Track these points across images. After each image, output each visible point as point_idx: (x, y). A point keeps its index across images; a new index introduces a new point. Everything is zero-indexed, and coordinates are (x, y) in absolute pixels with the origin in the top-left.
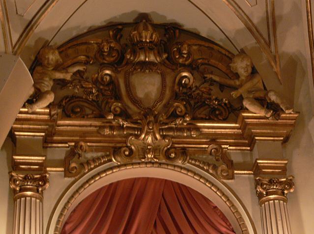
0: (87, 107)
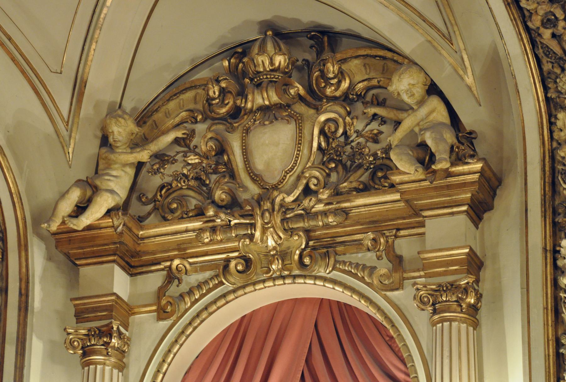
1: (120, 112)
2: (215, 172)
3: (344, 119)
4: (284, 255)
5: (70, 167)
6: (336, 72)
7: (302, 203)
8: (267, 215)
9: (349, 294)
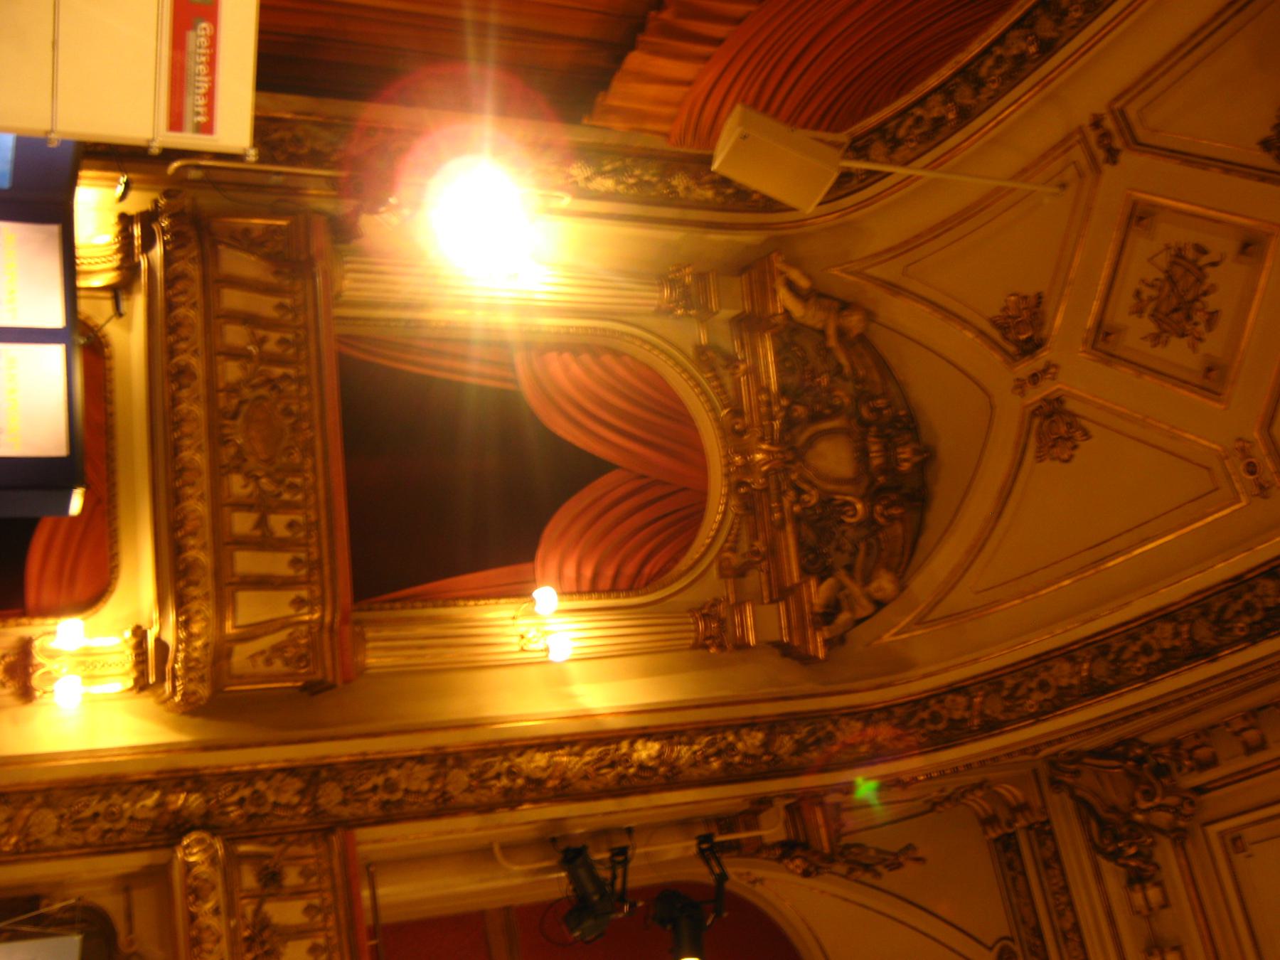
4: (748, 467)
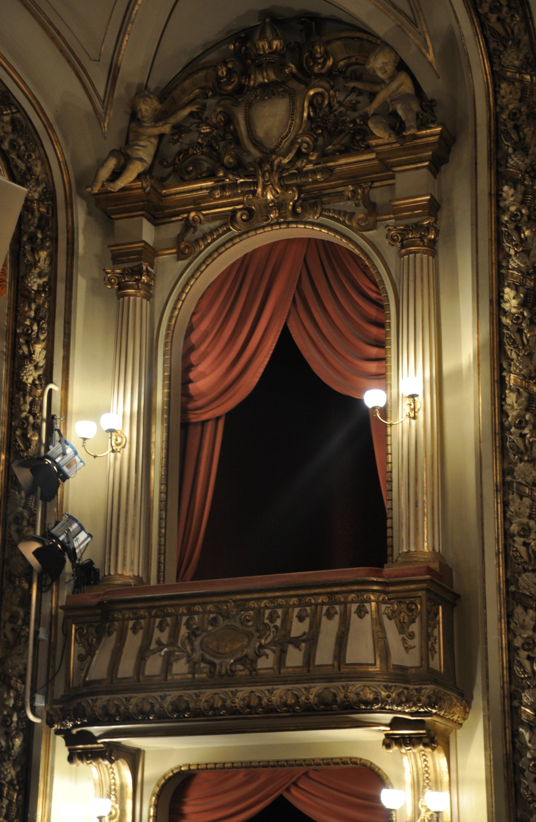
0: (205, 161)
1: (146, 92)
2: (224, 139)
3: (329, 92)
4: (280, 205)
5: (106, 139)
6: (322, 52)
7: (295, 164)
8: (267, 174)
9: (333, 235)
